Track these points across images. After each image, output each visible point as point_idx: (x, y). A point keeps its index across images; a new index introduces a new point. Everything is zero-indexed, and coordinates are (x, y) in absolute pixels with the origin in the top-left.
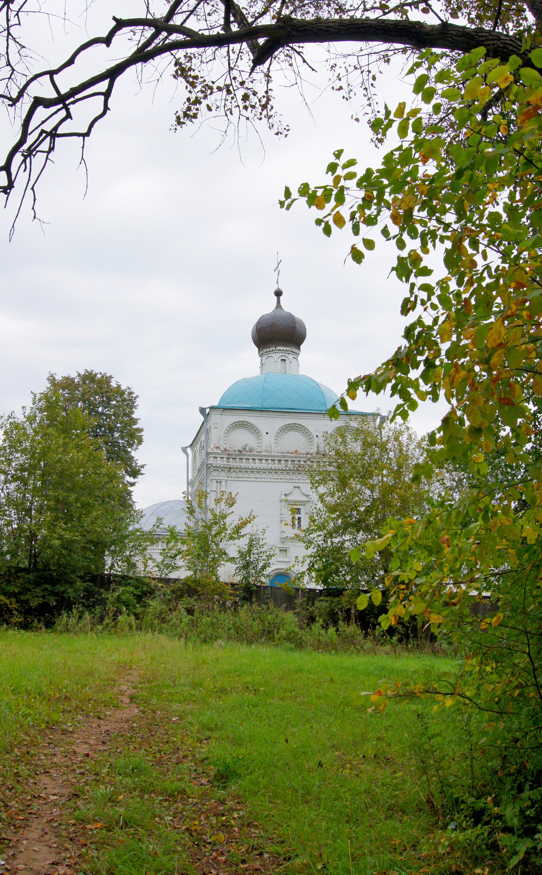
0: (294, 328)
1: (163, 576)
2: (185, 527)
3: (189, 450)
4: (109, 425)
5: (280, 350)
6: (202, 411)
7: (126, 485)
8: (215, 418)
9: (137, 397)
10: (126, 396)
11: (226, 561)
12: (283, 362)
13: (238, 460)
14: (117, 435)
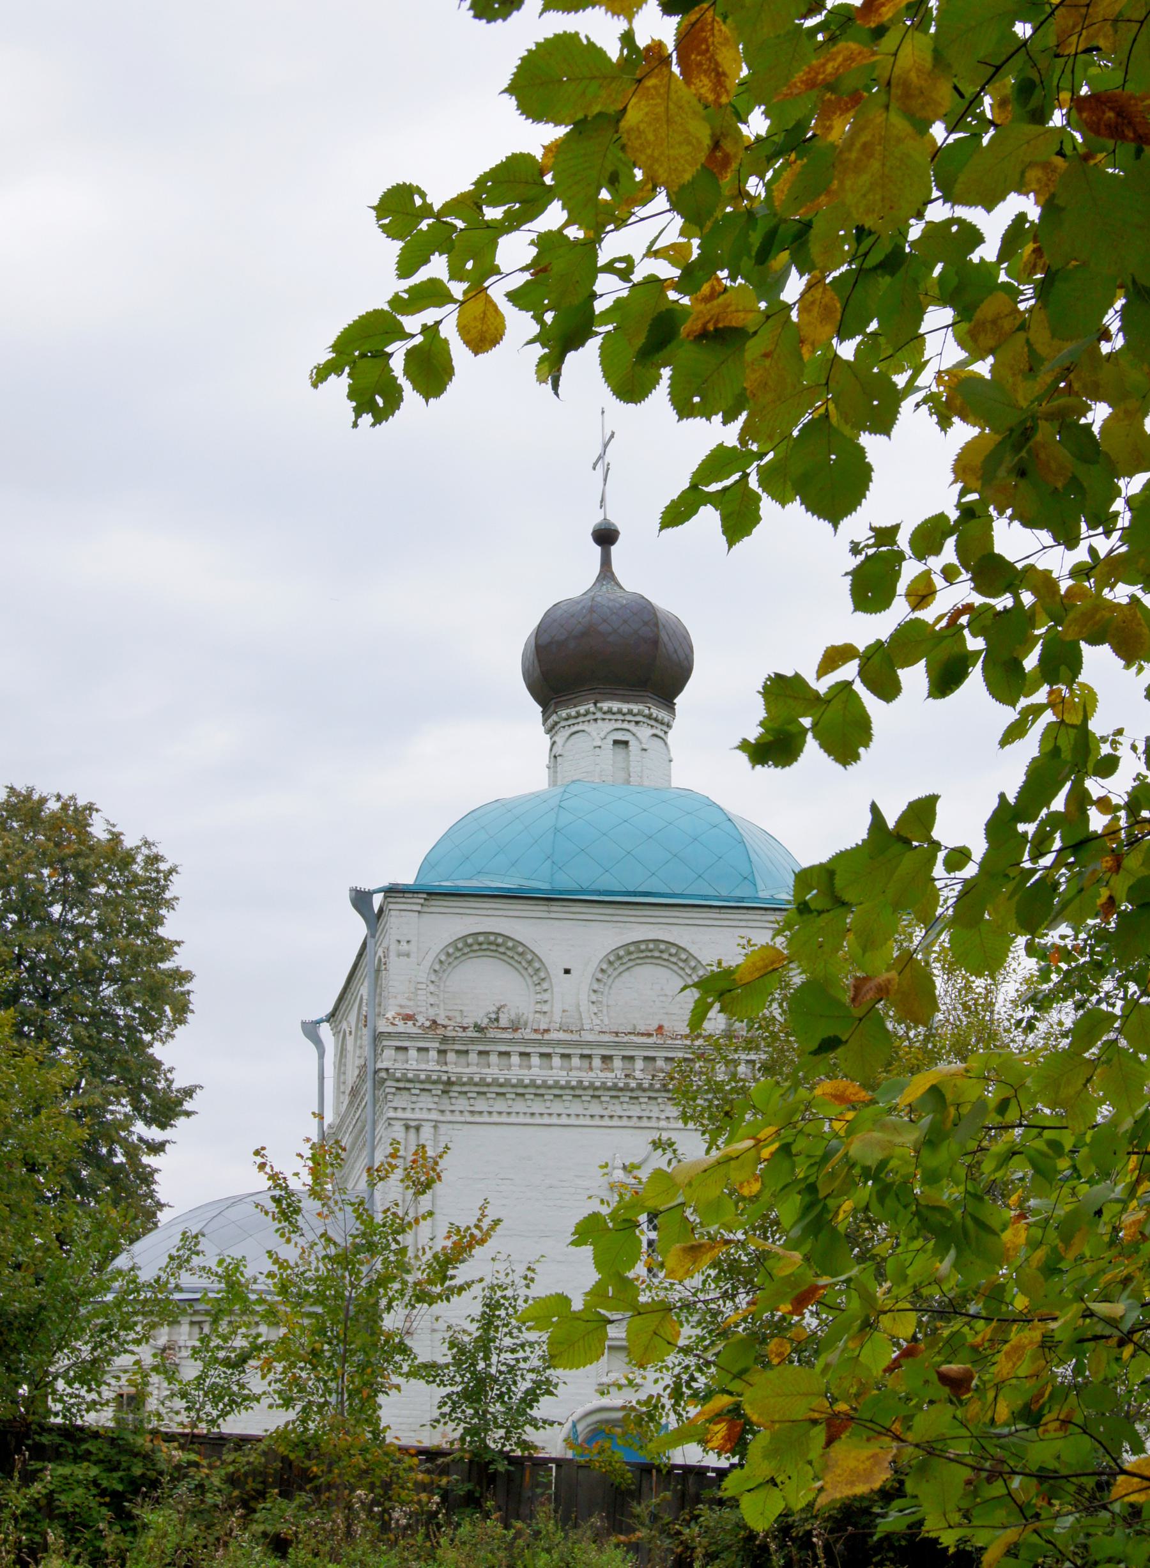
0: (655, 642)
1: (203, 1428)
2: (269, 1266)
3: (325, 1030)
4: (84, 960)
5: (610, 711)
6: (361, 899)
7: (136, 1148)
8: (403, 923)
9: (172, 871)
10: (137, 868)
11: (408, 1375)
12: (620, 750)
13: (473, 1057)
14: (108, 990)
